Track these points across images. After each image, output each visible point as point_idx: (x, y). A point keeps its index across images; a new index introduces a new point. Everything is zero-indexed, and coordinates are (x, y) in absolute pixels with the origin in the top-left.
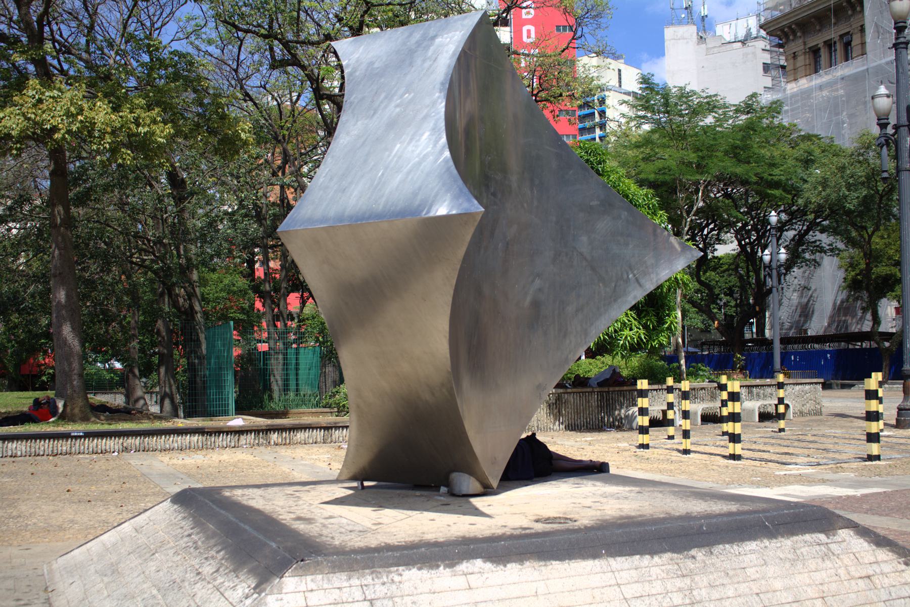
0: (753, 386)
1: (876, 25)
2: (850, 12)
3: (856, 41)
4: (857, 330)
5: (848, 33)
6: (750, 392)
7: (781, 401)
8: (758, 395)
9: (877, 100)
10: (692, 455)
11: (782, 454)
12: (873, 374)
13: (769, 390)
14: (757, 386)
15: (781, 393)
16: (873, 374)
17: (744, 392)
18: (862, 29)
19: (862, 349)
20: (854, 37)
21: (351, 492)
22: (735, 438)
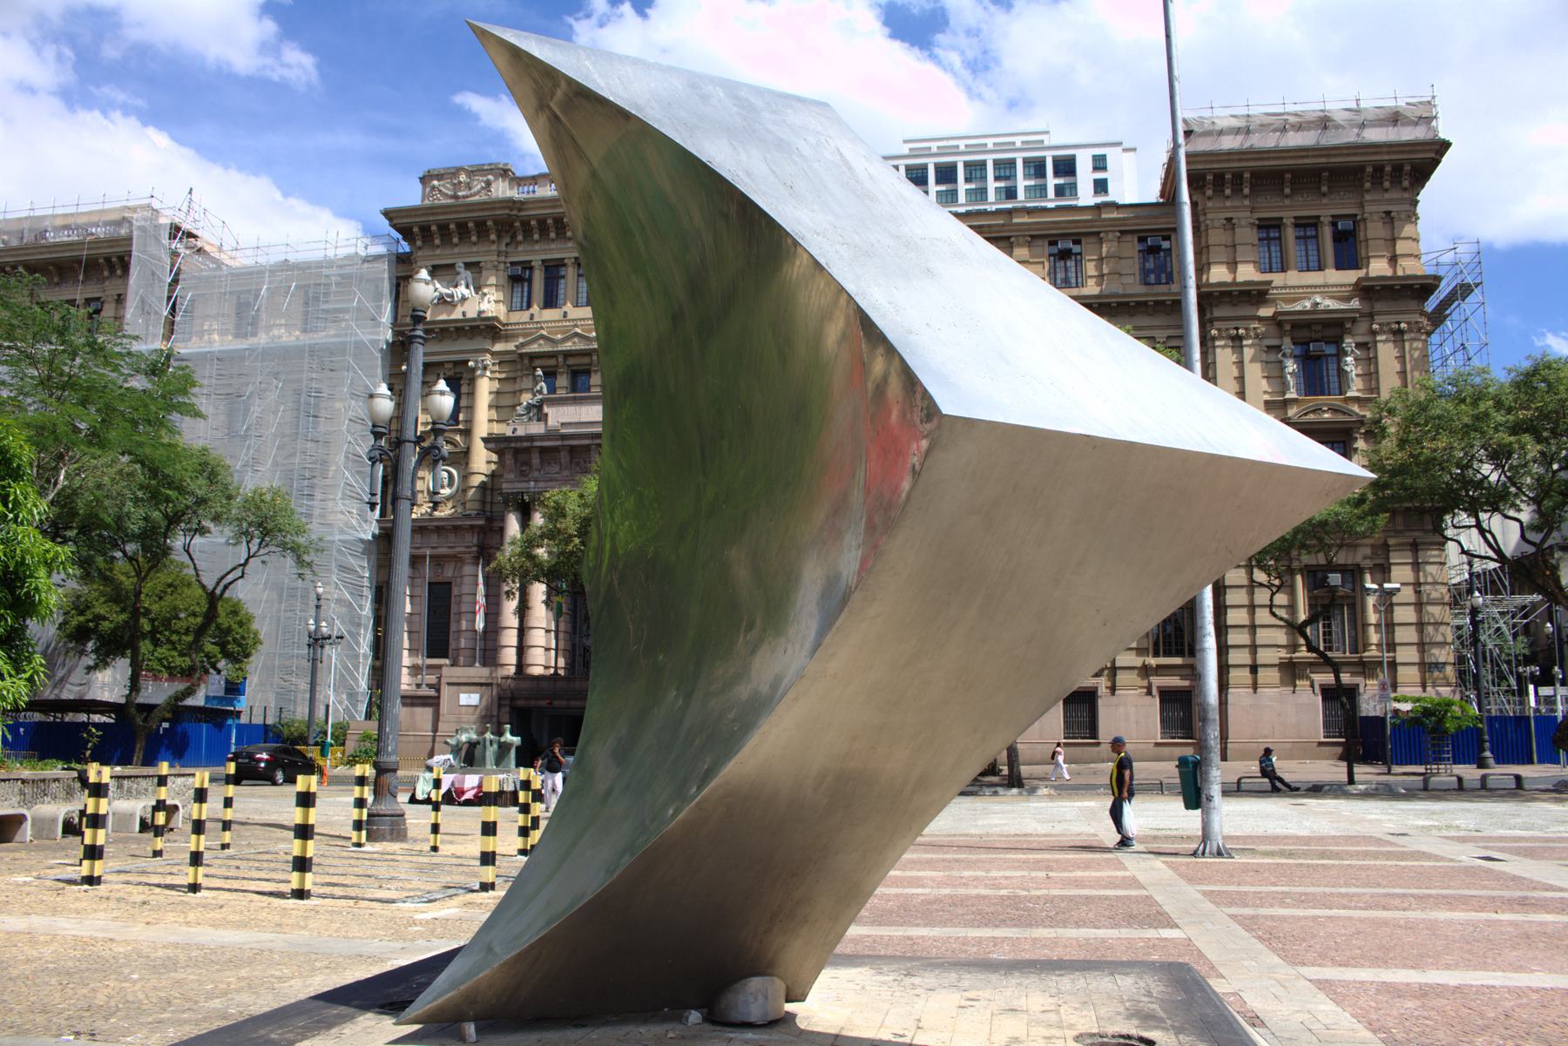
0: (124, 777)
1: (143, 301)
2: (106, 273)
3: (108, 311)
4: (52, 697)
5: (98, 299)
6: (120, 787)
7: (160, 806)
8: (129, 791)
9: (377, 400)
10: (203, 893)
11: (271, 894)
12: (300, 778)
13: (143, 783)
14: (129, 777)
15: (163, 793)
16: (300, 778)
17: (112, 784)
18: (120, 300)
19: (63, 723)
20: (106, 306)
21: (416, 1027)
22: (93, 853)
